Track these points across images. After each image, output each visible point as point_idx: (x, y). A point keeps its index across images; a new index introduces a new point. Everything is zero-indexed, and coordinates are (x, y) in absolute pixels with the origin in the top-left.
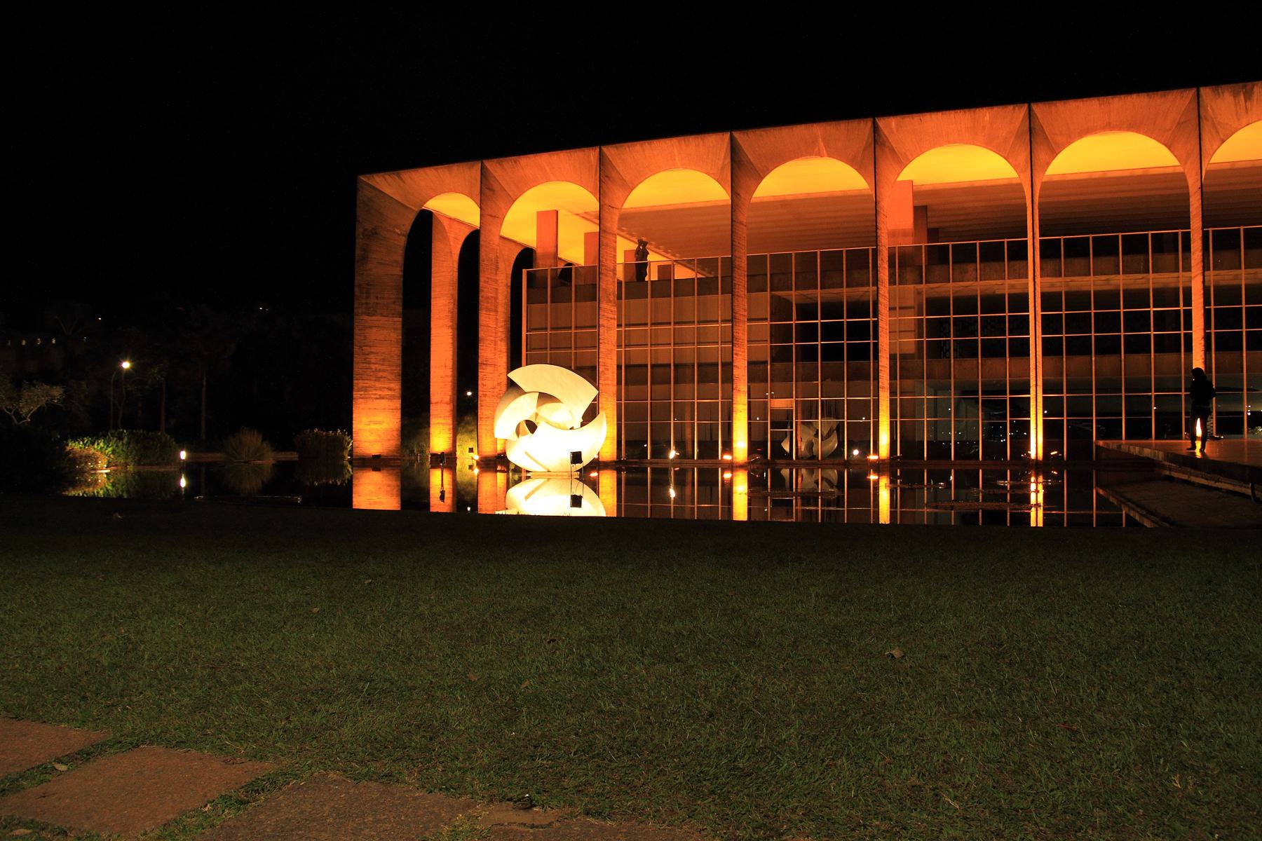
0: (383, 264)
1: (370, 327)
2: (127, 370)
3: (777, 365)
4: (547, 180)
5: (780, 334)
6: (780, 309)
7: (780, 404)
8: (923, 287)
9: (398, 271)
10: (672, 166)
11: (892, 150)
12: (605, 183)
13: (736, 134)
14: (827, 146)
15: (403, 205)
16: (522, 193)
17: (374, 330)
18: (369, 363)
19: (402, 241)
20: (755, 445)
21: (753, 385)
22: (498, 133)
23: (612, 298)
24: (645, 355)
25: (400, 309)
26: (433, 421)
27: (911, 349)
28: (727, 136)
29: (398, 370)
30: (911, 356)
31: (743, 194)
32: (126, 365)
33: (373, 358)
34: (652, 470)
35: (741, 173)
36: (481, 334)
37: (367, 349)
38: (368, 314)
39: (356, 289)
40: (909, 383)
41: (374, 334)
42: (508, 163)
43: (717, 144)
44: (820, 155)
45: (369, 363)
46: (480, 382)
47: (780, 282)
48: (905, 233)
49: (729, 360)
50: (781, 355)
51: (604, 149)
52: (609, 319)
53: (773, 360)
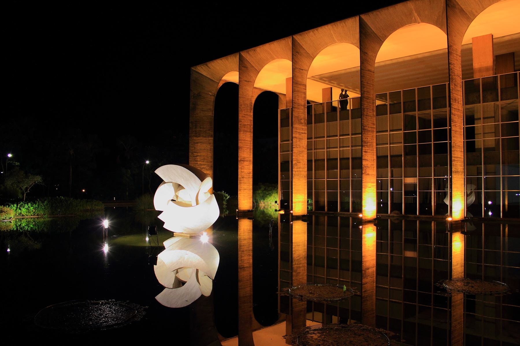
0: (205, 110)
1: (197, 143)
2: (148, 164)
3: (408, 157)
4: (273, 59)
5: (408, 138)
6: (409, 123)
7: (410, 180)
8: (500, 103)
9: (211, 114)
10: (333, 42)
11: (462, 11)
12: (299, 57)
13: (363, 16)
14: (419, 15)
15: (212, 80)
16: (262, 67)
17: (199, 144)
18: (197, 161)
19: (213, 99)
20: (381, 207)
21: (380, 170)
22: (246, 36)
23: (303, 121)
24: (323, 153)
25: (212, 133)
26: (374, 262)
27: (492, 144)
28: (357, 18)
29: (211, 164)
30: (493, 149)
31: (370, 54)
32: (148, 162)
33: (198, 158)
34: (341, 218)
35: (368, 42)
36: (240, 145)
37: (195, 154)
38: (196, 136)
39: (190, 124)
40: (491, 167)
41: (199, 146)
42: (251, 51)
43: (351, 25)
44: (416, 22)
45: (197, 161)
46: (239, 170)
47: (409, 106)
48: (487, 69)
49: (359, 155)
50: (409, 151)
51: (294, 37)
52: (300, 133)
53: (406, 154)
